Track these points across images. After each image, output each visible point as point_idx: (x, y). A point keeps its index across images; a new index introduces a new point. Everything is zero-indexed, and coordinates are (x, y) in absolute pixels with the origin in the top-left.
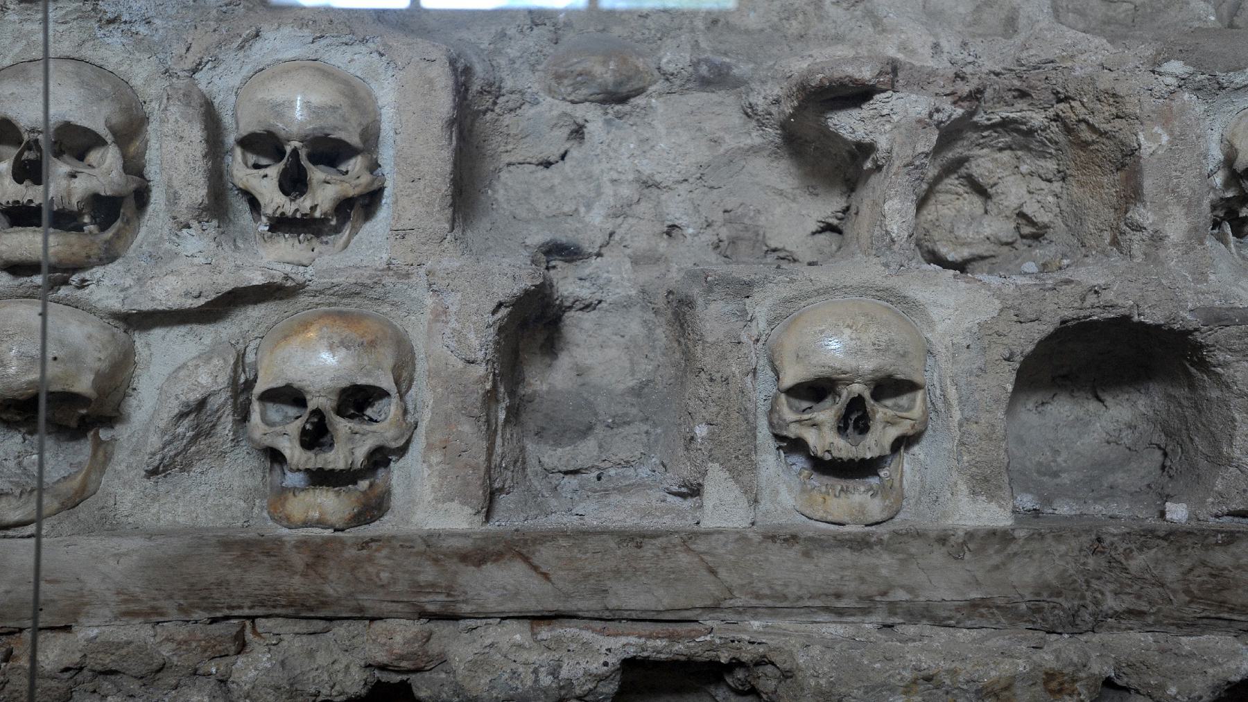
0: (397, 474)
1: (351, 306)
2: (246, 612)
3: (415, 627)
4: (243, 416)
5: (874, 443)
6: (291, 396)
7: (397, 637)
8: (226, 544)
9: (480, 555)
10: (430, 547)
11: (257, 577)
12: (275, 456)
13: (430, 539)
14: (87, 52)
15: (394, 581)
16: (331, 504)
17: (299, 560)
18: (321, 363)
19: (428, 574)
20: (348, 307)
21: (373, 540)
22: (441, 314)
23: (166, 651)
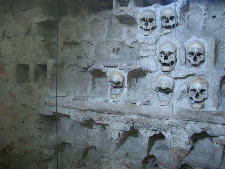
0: (206, 102)
1: (201, 77)
2: (188, 120)
3: (208, 124)
4: (188, 92)
5: (200, 100)
6: (194, 90)
7: (205, 125)
8: (186, 110)
9: (217, 115)
10: (211, 113)
11: (189, 115)
12: (191, 98)
13: (211, 112)
14: (171, 40)
15: (206, 117)
16: (198, 106)
17: (194, 113)
18: (198, 86)
19: (210, 117)
20: (201, 77)
21: (204, 111)
22: (213, 79)
23: (179, 124)
